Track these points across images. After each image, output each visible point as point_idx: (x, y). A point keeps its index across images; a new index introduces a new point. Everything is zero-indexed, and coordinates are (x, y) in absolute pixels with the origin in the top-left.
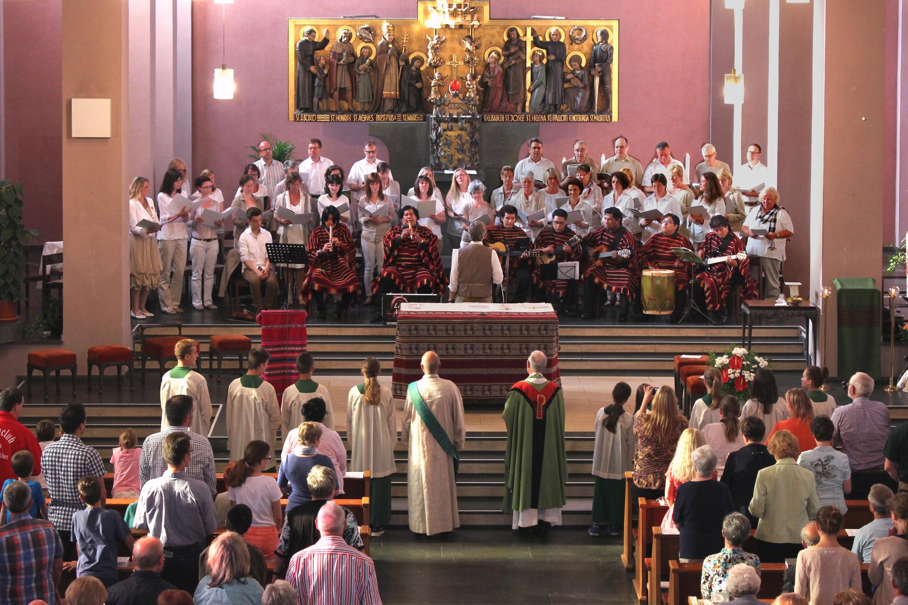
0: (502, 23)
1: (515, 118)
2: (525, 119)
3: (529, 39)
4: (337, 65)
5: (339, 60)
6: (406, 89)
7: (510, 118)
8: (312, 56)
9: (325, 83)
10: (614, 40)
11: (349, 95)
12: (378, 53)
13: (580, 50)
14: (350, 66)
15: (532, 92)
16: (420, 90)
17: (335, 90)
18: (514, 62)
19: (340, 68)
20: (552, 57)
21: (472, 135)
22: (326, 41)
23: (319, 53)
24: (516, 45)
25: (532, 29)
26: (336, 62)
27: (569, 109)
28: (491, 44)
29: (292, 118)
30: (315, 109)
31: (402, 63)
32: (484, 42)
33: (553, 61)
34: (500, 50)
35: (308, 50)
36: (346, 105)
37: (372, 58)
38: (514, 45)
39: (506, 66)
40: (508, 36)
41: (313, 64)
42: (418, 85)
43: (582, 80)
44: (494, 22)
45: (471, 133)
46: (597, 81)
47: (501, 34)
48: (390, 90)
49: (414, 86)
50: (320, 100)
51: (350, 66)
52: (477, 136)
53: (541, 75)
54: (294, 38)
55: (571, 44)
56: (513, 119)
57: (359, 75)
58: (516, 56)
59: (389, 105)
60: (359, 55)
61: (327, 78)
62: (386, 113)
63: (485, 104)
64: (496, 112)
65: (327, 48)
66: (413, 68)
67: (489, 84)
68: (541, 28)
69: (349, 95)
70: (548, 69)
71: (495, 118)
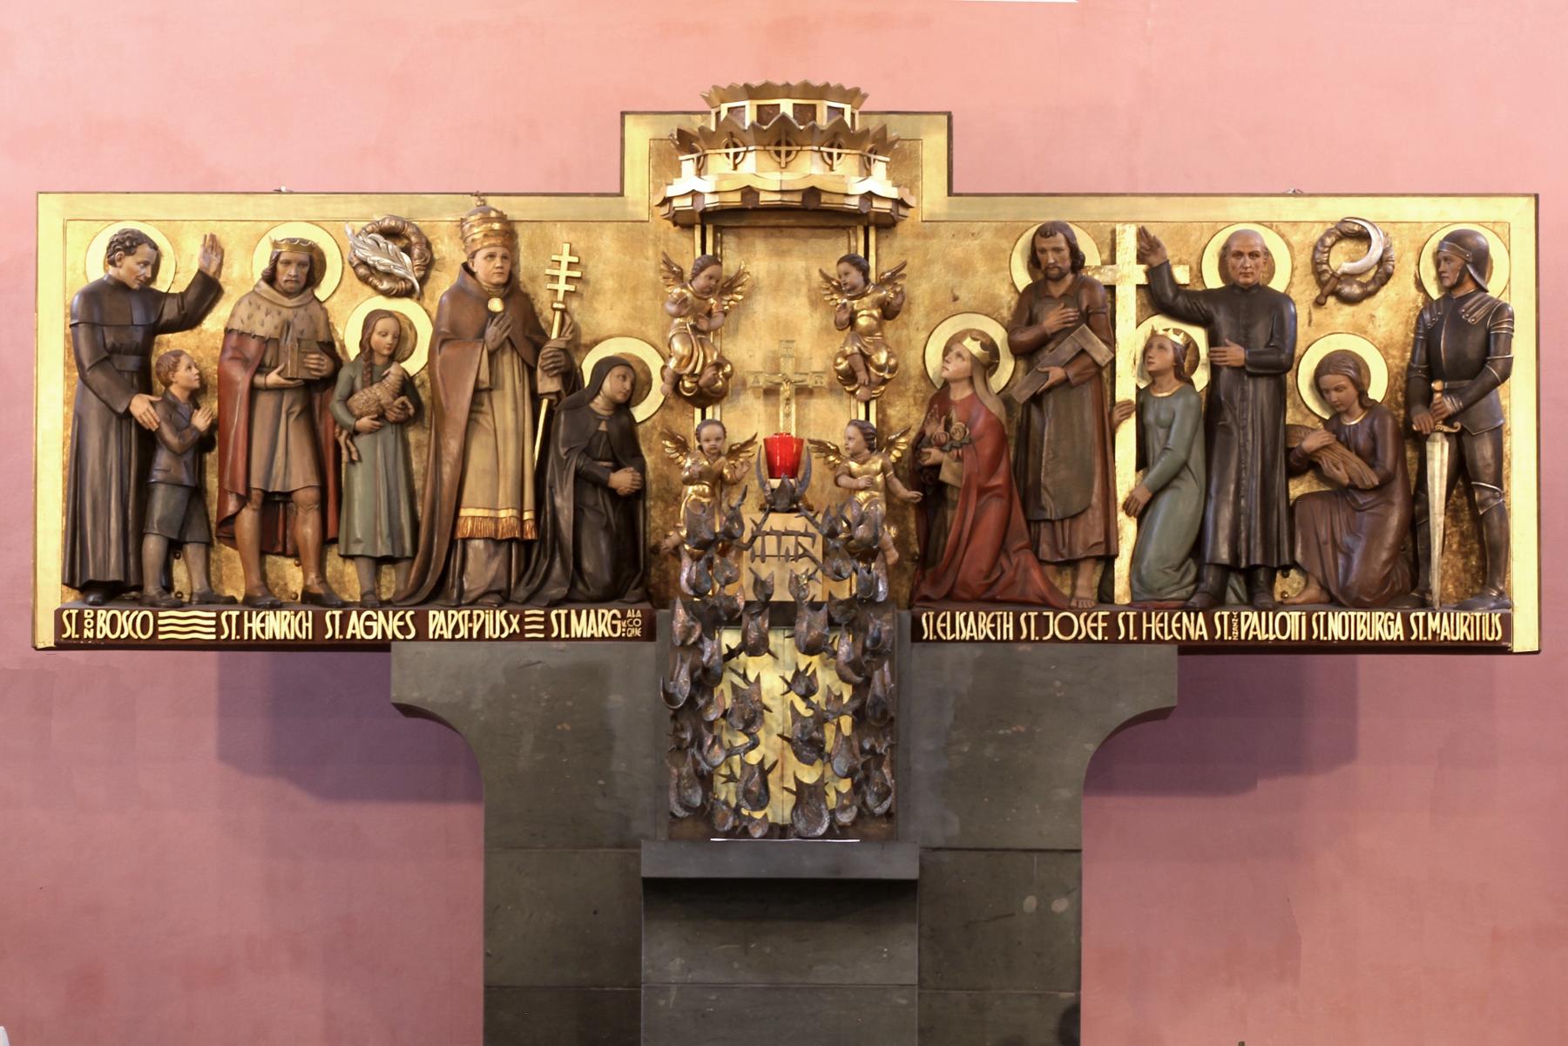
0: (1008, 210)
1: (1066, 625)
2: (1112, 629)
3: (1129, 276)
4: (254, 390)
5: (262, 369)
6: (564, 503)
7: (1043, 624)
8: (145, 351)
9: (199, 470)
10: (1511, 280)
11: (307, 529)
12: (441, 340)
13: (1360, 331)
14: (313, 392)
15: (1142, 512)
16: (630, 505)
17: (244, 500)
18: (1057, 374)
19: (265, 403)
20: (1235, 354)
21: (858, 672)
22: (207, 289)
23: (172, 341)
24: (1070, 297)
25: (1142, 234)
26: (241, 377)
27: (1313, 591)
28: (952, 304)
29: (46, 637)
30: (152, 589)
31: (548, 385)
32: (921, 290)
33: (1238, 370)
34: (998, 334)
35: (125, 325)
36: (293, 576)
37: (415, 364)
38: (1059, 297)
39: (1022, 396)
40: (1035, 261)
41: (147, 389)
42: (622, 480)
43: (1370, 457)
44: (965, 208)
45: (854, 665)
46: (1439, 457)
47: (1000, 261)
48: (491, 503)
49: (602, 485)
50: (174, 548)
51: (313, 392)
52: (882, 678)
53: (1182, 435)
54: (73, 261)
55: (1319, 303)
56: (1054, 628)
57: (355, 433)
58: (1067, 349)
59: (480, 569)
60: (353, 351)
61: (211, 458)
62: (473, 604)
63: (932, 573)
64: (986, 598)
65: (215, 322)
66: (599, 404)
67: (946, 475)
68: (1181, 231)
69: (307, 529)
70: (1213, 410)
71: (972, 625)
